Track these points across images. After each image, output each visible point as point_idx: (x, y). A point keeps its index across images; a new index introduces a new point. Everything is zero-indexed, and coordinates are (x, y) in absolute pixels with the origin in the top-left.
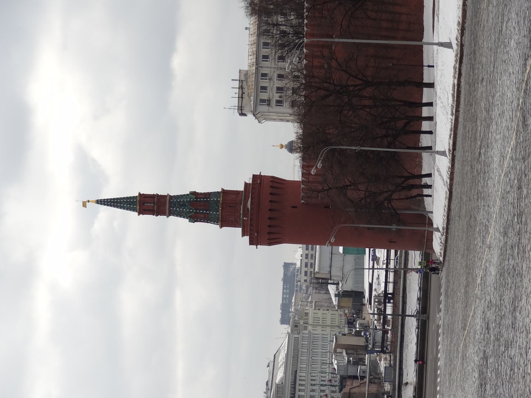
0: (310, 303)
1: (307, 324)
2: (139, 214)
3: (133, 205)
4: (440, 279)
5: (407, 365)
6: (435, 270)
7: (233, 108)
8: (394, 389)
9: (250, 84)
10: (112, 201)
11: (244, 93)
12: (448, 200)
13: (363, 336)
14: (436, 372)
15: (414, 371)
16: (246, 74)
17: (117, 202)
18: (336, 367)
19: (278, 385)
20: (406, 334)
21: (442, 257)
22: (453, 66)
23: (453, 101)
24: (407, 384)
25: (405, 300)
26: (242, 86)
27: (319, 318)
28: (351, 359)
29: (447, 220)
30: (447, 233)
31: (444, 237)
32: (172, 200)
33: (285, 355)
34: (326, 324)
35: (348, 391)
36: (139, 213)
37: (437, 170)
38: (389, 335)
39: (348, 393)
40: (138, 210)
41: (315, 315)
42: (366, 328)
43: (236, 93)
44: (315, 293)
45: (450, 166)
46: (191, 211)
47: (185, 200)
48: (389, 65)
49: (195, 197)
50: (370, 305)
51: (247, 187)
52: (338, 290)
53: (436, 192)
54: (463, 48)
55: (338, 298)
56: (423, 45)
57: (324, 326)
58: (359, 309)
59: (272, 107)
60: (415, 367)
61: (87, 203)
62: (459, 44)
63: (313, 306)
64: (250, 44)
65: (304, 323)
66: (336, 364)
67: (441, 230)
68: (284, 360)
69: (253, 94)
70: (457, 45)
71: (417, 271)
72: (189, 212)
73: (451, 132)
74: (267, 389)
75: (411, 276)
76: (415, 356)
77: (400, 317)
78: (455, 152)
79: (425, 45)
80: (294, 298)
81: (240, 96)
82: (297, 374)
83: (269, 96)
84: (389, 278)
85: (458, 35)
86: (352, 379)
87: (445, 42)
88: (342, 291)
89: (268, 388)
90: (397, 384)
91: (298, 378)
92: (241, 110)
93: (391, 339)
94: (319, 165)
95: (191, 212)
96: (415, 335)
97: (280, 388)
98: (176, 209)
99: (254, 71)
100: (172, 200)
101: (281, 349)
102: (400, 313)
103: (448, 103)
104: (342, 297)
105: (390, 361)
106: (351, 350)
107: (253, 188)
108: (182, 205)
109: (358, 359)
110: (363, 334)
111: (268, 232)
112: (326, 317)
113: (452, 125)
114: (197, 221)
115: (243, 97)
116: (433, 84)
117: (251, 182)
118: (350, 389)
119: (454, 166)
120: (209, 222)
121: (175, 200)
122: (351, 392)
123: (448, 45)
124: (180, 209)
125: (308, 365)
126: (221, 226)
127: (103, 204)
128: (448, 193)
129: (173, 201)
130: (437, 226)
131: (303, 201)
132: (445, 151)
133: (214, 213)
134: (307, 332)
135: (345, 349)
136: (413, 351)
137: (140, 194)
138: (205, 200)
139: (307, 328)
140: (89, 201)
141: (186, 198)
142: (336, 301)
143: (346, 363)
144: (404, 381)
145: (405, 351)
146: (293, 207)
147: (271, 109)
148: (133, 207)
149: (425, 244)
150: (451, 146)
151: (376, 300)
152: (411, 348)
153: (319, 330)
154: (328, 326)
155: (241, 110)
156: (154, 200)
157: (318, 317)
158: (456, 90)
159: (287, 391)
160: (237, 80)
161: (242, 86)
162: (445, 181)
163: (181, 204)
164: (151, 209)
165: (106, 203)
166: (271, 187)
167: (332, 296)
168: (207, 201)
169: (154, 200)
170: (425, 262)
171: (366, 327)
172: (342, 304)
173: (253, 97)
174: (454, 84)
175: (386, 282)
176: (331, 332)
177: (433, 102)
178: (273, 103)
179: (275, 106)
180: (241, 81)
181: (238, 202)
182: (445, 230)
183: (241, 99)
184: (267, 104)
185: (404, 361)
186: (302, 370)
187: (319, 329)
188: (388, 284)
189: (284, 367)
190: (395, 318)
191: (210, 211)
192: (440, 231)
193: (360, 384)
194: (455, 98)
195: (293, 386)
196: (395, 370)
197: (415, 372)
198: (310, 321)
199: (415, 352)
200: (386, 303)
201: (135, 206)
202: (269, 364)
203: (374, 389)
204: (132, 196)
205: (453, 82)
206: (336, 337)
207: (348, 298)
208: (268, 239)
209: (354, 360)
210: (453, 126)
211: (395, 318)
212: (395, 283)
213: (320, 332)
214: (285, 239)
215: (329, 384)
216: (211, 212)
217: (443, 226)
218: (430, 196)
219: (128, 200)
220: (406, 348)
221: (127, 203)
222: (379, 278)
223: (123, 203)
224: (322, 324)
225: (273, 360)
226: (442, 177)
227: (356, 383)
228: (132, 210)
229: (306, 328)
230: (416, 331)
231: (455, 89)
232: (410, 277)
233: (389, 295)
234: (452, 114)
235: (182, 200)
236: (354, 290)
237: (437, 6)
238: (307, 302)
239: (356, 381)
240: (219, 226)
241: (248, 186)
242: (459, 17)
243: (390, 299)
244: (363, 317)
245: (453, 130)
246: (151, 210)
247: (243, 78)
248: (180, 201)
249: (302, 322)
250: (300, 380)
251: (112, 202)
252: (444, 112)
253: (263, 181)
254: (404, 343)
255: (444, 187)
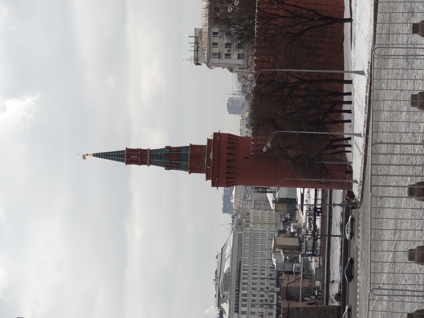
0: (250, 202)
1: (249, 222)
2: (127, 164)
3: (122, 158)
4: (359, 212)
5: (333, 267)
6: (355, 206)
7: (190, 59)
8: (323, 286)
9: (203, 40)
10: (106, 154)
11: (199, 47)
12: (363, 164)
13: (296, 237)
14: (356, 290)
15: (339, 271)
16: (201, 31)
17: (109, 155)
18: (275, 264)
19: (225, 274)
20: (332, 242)
21: (360, 199)
22: (366, 85)
23: (366, 105)
24: (333, 282)
25: (331, 214)
26: (197, 42)
27: (259, 217)
28: (287, 257)
29: (363, 177)
30: (363, 184)
31: (361, 187)
32: (152, 154)
33: (231, 248)
34: (264, 222)
35: (286, 286)
36: (127, 163)
37: (355, 143)
38: (319, 241)
39: (286, 288)
40: (126, 161)
41: (255, 214)
42: (299, 230)
43: (192, 47)
44: (254, 192)
45: (365, 144)
46: (167, 161)
47: (162, 153)
48: (315, 19)
49: (169, 150)
50: (302, 212)
51: (209, 143)
52: (275, 198)
53: (355, 156)
54: (364, 181)
55: (275, 205)
56: (344, 73)
57: (263, 224)
58: (293, 211)
59: (222, 59)
60: (340, 268)
61: (86, 156)
62: (369, 74)
63: (253, 204)
64: (203, 8)
65: (246, 222)
66: (275, 262)
67: (359, 182)
68: (230, 253)
69: (206, 49)
70: (368, 74)
71: (340, 205)
72: (165, 162)
73: (365, 123)
74: (217, 277)
75: (336, 195)
76: (340, 260)
77: (327, 237)
78: (368, 136)
79: (346, 73)
80: (234, 191)
81: (196, 49)
82: (241, 265)
83: (220, 50)
84: (318, 194)
85: (369, 69)
86: (288, 274)
87: (359, 71)
88: (279, 198)
89: (217, 276)
90: (325, 282)
91: (242, 268)
92: (197, 60)
93: (320, 245)
94: (269, 145)
95: (167, 162)
96: (340, 243)
97: (227, 276)
98: (155, 160)
99: (207, 31)
100: (152, 154)
101: (227, 244)
102: (327, 234)
103: (362, 105)
104: (279, 203)
105: (320, 262)
106: (287, 250)
107: (214, 144)
108: (159, 157)
109: (293, 257)
110: (296, 235)
111: (227, 177)
112: (264, 216)
113: (365, 120)
114: (171, 169)
115: (198, 50)
116: (352, 81)
117: (212, 138)
118: (287, 284)
119: (368, 144)
120: (180, 169)
121: (154, 153)
122: (288, 286)
123: (362, 73)
124: (158, 160)
125: (250, 257)
126: (190, 173)
127: (98, 157)
128: (363, 160)
129: (153, 154)
130: (356, 179)
131: (252, 153)
132: (361, 133)
133: (185, 163)
134: (249, 229)
135: (282, 249)
136: (338, 256)
137: (127, 149)
138: (177, 153)
139: (249, 225)
140: (87, 155)
141: (162, 152)
142: (273, 206)
143: (284, 261)
144: (331, 280)
145: (332, 255)
146: (245, 158)
147: (221, 61)
148: (122, 159)
149: (347, 185)
150: (365, 132)
151: (308, 214)
152: (336, 253)
153: (259, 227)
154: (266, 223)
155: (197, 60)
156: (138, 154)
157: (257, 216)
158: (368, 99)
159: (233, 279)
160: (193, 37)
161: (197, 42)
162: (361, 152)
163: (159, 156)
164: (136, 160)
165: (101, 156)
166: (228, 142)
167: (270, 201)
168: (179, 153)
169: (138, 154)
170: (347, 201)
171: (299, 229)
172: (279, 209)
173: (207, 51)
174: (366, 96)
175: (316, 200)
176: (269, 229)
177: (351, 92)
178: (223, 56)
179: (224, 58)
180: (196, 37)
181: (203, 154)
182: (362, 183)
183: (196, 52)
184: (218, 57)
185: (331, 263)
186: (246, 260)
187: (259, 226)
188: (317, 200)
189: (230, 259)
190: (323, 228)
191: (181, 162)
192: (358, 183)
193: (295, 279)
194: (368, 104)
195: (238, 275)
196: (324, 271)
197: (340, 272)
198: (251, 220)
199: (339, 256)
200: (316, 216)
201: (123, 158)
202: (217, 256)
203: (307, 283)
204: (121, 150)
205: (365, 95)
206: (274, 239)
207: (284, 204)
208: (226, 183)
209: (290, 258)
210: (366, 120)
211: (323, 228)
212: (323, 200)
213: (260, 229)
214: (239, 182)
215: (269, 277)
216: (182, 162)
217: (360, 180)
218: (350, 152)
219: (118, 154)
220: (332, 253)
221: (117, 156)
222: (309, 192)
223: (114, 156)
224: (261, 222)
225: (221, 253)
226: (359, 149)
227: (292, 278)
228: (121, 161)
229: (247, 226)
230: (340, 239)
231: (367, 99)
232: (335, 196)
233: (318, 210)
234: (366, 113)
235: (159, 153)
236: (288, 197)
237: (354, 37)
238: (248, 201)
239: (292, 275)
240: (188, 172)
241: (210, 141)
242: (369, 59)
243: (319, 212)
244: (296, 220)
245: (366, 122)
246: (136, 161)
247: (198, 35)
248: (158, 154)
249: (244, 221)
250: (244, 270)
251: (106, 155)
252: (359, 109)
253: (221, 139)
254: (331, 249)
255: (360, 155)
